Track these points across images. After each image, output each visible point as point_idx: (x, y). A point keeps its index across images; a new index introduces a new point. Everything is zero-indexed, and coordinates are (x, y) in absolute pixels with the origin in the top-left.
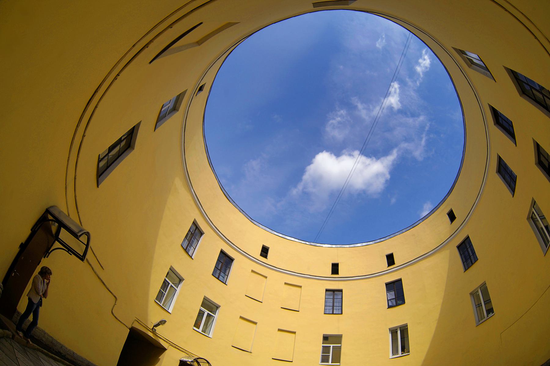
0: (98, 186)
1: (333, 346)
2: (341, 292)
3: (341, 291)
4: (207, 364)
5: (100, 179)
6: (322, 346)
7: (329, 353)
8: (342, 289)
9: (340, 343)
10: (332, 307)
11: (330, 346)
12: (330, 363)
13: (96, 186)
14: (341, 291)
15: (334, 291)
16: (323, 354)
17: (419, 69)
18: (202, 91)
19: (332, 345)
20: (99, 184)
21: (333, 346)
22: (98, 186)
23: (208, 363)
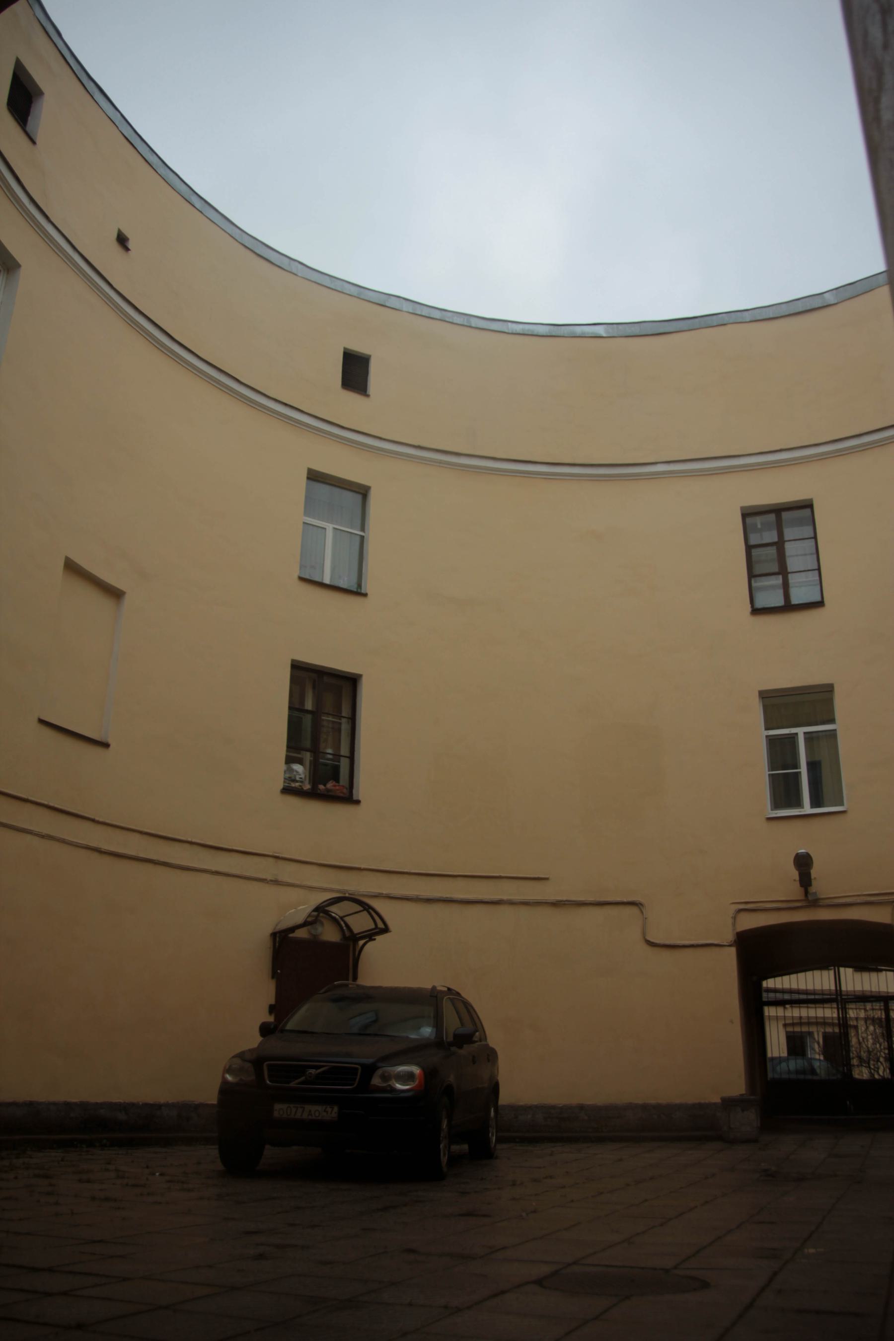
0: (34, 143)
1: (805, 733)
2: (808, 511)
3: (808, 505)
4: (365, 912)
5: (28, 129)
6: (767, 736)
7: (796, 765)
8: (811, 500)
9: (832, 721)
10: (786, 538)
11: (797, 734)
12: (807, 809)
13: (30, 143)
14: (808, 505)
15: (778, 511)
16: (772, 771)
17: (806, 1250)
18: (41, 93)
19: (800, 731)
20: (35, 140)
21: (805, 733)
22: (34, 143)
23: (365, 909)
